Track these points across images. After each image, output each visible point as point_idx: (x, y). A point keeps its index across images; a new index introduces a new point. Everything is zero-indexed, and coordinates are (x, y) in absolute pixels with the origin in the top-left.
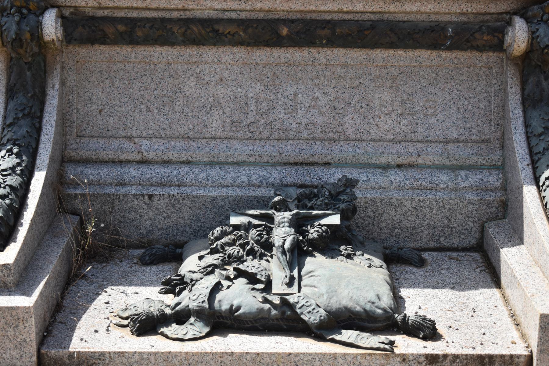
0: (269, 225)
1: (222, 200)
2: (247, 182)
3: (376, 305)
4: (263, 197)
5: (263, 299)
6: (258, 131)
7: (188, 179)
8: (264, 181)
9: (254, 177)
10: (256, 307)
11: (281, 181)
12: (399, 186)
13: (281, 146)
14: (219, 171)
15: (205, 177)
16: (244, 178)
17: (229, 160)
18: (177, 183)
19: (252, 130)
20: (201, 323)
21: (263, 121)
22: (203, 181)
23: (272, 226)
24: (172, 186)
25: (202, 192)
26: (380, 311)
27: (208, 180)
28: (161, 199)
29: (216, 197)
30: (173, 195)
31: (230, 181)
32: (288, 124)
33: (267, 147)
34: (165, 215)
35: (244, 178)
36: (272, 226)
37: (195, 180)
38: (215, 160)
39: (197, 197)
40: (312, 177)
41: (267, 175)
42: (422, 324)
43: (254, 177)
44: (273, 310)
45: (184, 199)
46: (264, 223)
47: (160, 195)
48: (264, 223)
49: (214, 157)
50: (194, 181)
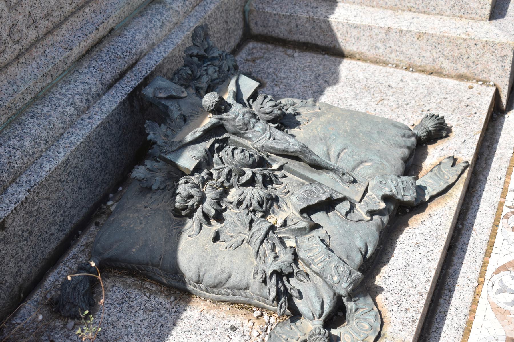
0: (221, 137)
1: (75, 157)
2: (76, 113)
3: (407, 135)
4: (107, 117)
5: (369, 215)
6: (24, 36)
7: (19, 162)
8: (89, 97)
9: (77, 98)
10: (374, 228)
11: (102, 84)
12: (185, 13)
13: (60, 38)
14: (37, 122)
15: (33, 143)
16: (70, 110)
17: (28, 99)
18: (10, 179)
19: (16, 39)
20: (360, 298)
21: (21, 17)
22: (35, 151)
23: (226, 135)
24: (8, 187)
25: (48, 167)
26: (425, 137)
27: (39, 144)
28: (15, 216)
29: (68, 160)
30: (26, 198)
31: (60, 125)
32: (46, 4)
33: (48, 51)
34: (25, 234)
35: (70, 110)
36: (226, 135)
37: (26, 156)
38: (14, 111)
39: (50, 177)
40: (122, 56)
41: (86, 87)
42: (439, 123)
43: (77, 98)
44: (383, 218)
45: (38, 193)
46: (212, 140)
47: (12, 212)
48: (212, 140)
49: (10, 108)
50: (26, 160)
